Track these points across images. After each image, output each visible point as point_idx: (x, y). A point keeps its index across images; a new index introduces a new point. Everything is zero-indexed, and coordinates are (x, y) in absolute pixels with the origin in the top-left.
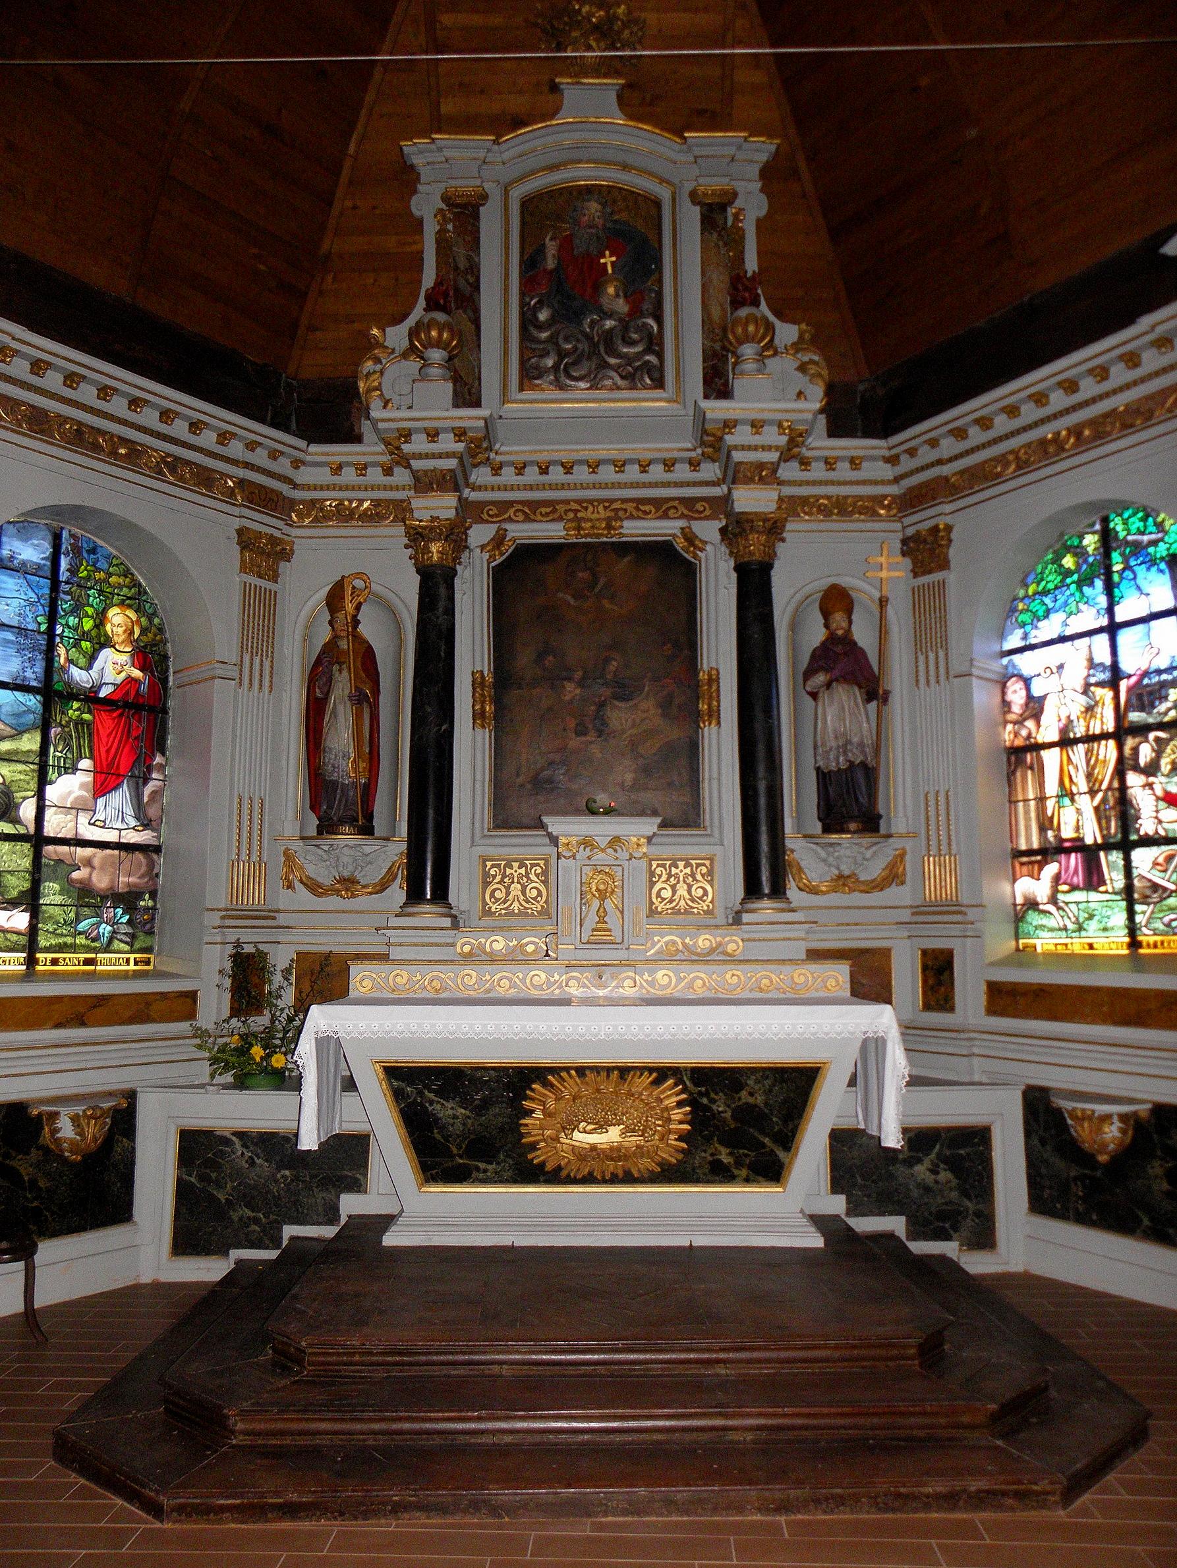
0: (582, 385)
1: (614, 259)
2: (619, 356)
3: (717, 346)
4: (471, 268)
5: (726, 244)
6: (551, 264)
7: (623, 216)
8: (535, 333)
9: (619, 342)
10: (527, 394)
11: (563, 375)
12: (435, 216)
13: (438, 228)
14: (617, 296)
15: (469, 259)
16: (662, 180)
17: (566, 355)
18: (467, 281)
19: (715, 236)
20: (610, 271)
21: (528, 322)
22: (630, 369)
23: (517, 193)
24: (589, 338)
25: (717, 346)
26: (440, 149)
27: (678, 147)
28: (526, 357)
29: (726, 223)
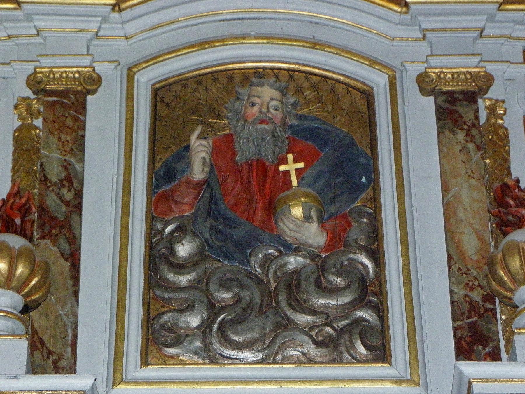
0: (248, 355)
1: (301, 165)
2: (312, 312)
3: (477, 296)
4: (69, 178)
5: (479, 148)
6: (198, 173)
7: (313, 110)
8: (171, 276)
9: (312, 288)
10: (154, 371)
11: (216, 337)
12: (16, 107)
13: (18, 123)
14: (307, 218)
15: (66, 166)
16: (373, 62)
17: (222, 309)
18: (61, 198)
19: (461, 136)
20: (295, 183)
21: (158, 257)
22: (329, 329)
23: (146, 79)
24: (258, 281)
25: (477, 296)
26: (29, 17)
27: (397, 18)
28: (153, 313)
29: (477, 118)
